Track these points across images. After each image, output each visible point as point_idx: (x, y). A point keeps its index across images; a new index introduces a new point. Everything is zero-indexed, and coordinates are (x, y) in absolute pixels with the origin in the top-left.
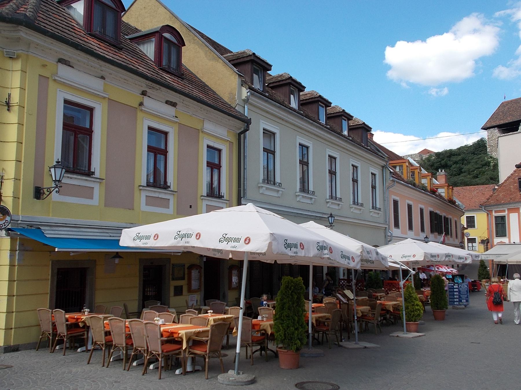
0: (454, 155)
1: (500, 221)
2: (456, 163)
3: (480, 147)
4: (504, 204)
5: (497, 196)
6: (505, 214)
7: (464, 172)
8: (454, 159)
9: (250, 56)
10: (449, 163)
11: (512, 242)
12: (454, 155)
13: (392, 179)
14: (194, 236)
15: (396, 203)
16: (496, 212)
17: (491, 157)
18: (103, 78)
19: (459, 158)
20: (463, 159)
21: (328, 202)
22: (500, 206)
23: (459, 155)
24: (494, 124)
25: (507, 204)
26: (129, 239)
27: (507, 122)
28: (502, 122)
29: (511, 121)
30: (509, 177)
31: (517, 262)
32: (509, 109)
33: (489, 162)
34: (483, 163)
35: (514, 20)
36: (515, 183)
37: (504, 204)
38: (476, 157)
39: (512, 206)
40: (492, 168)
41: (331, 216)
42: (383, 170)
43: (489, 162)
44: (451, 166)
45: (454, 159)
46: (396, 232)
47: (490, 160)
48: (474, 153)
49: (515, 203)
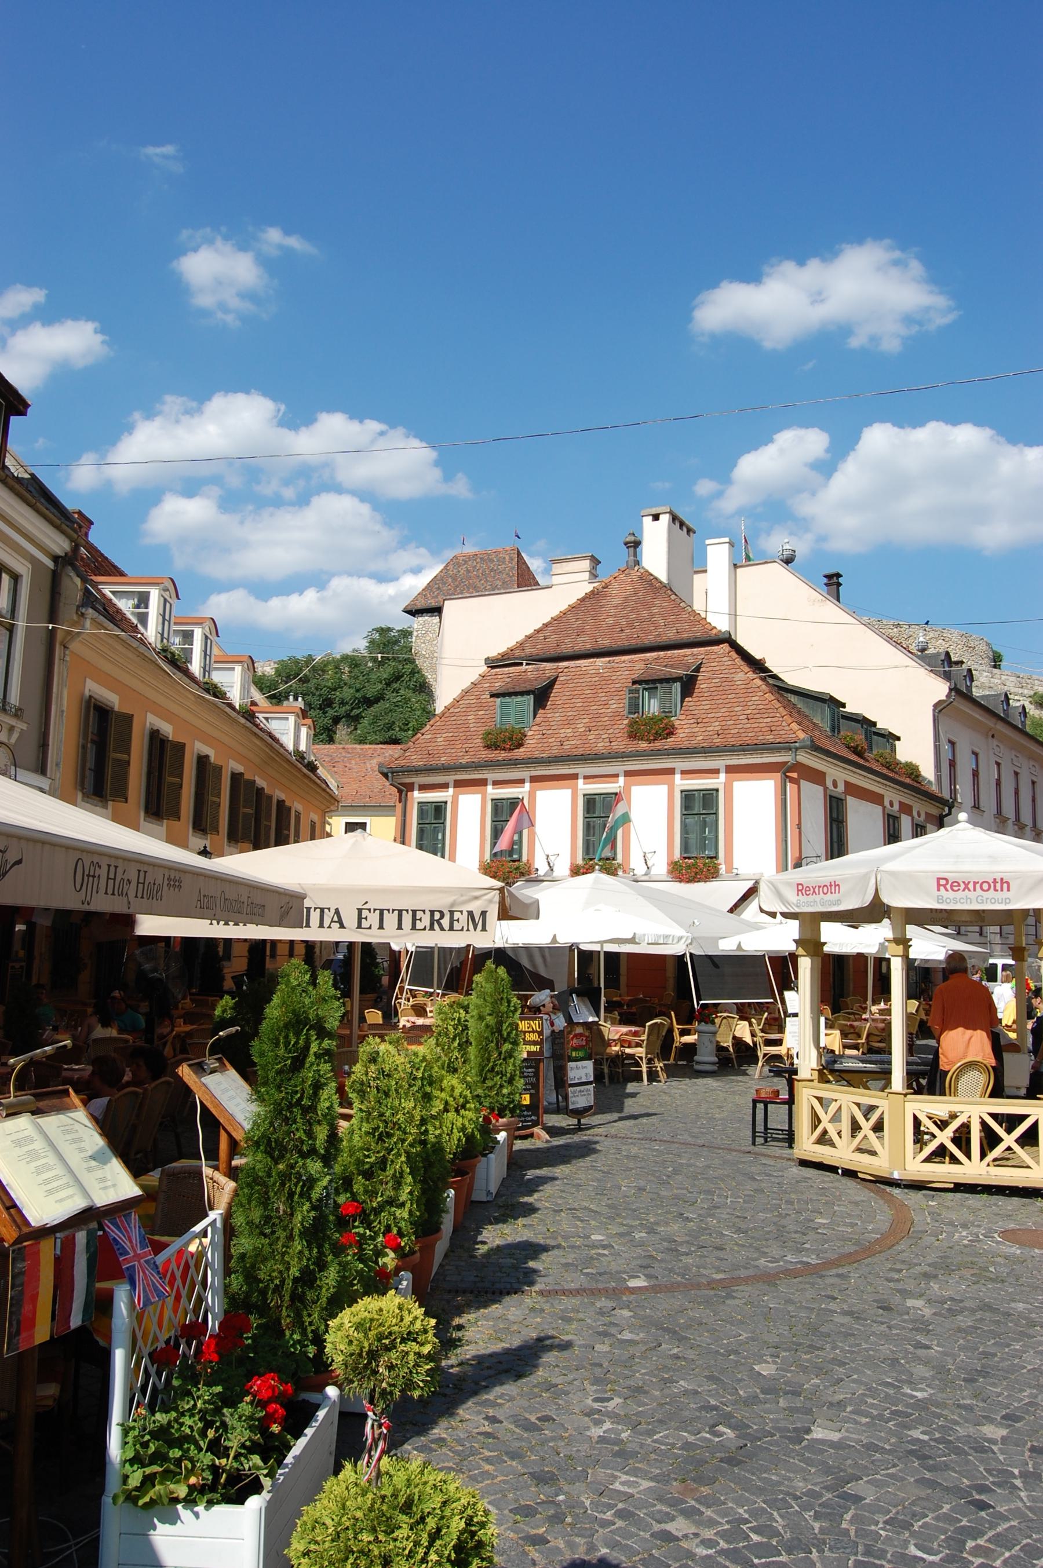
16: (423, 788)
32: (468, 571)
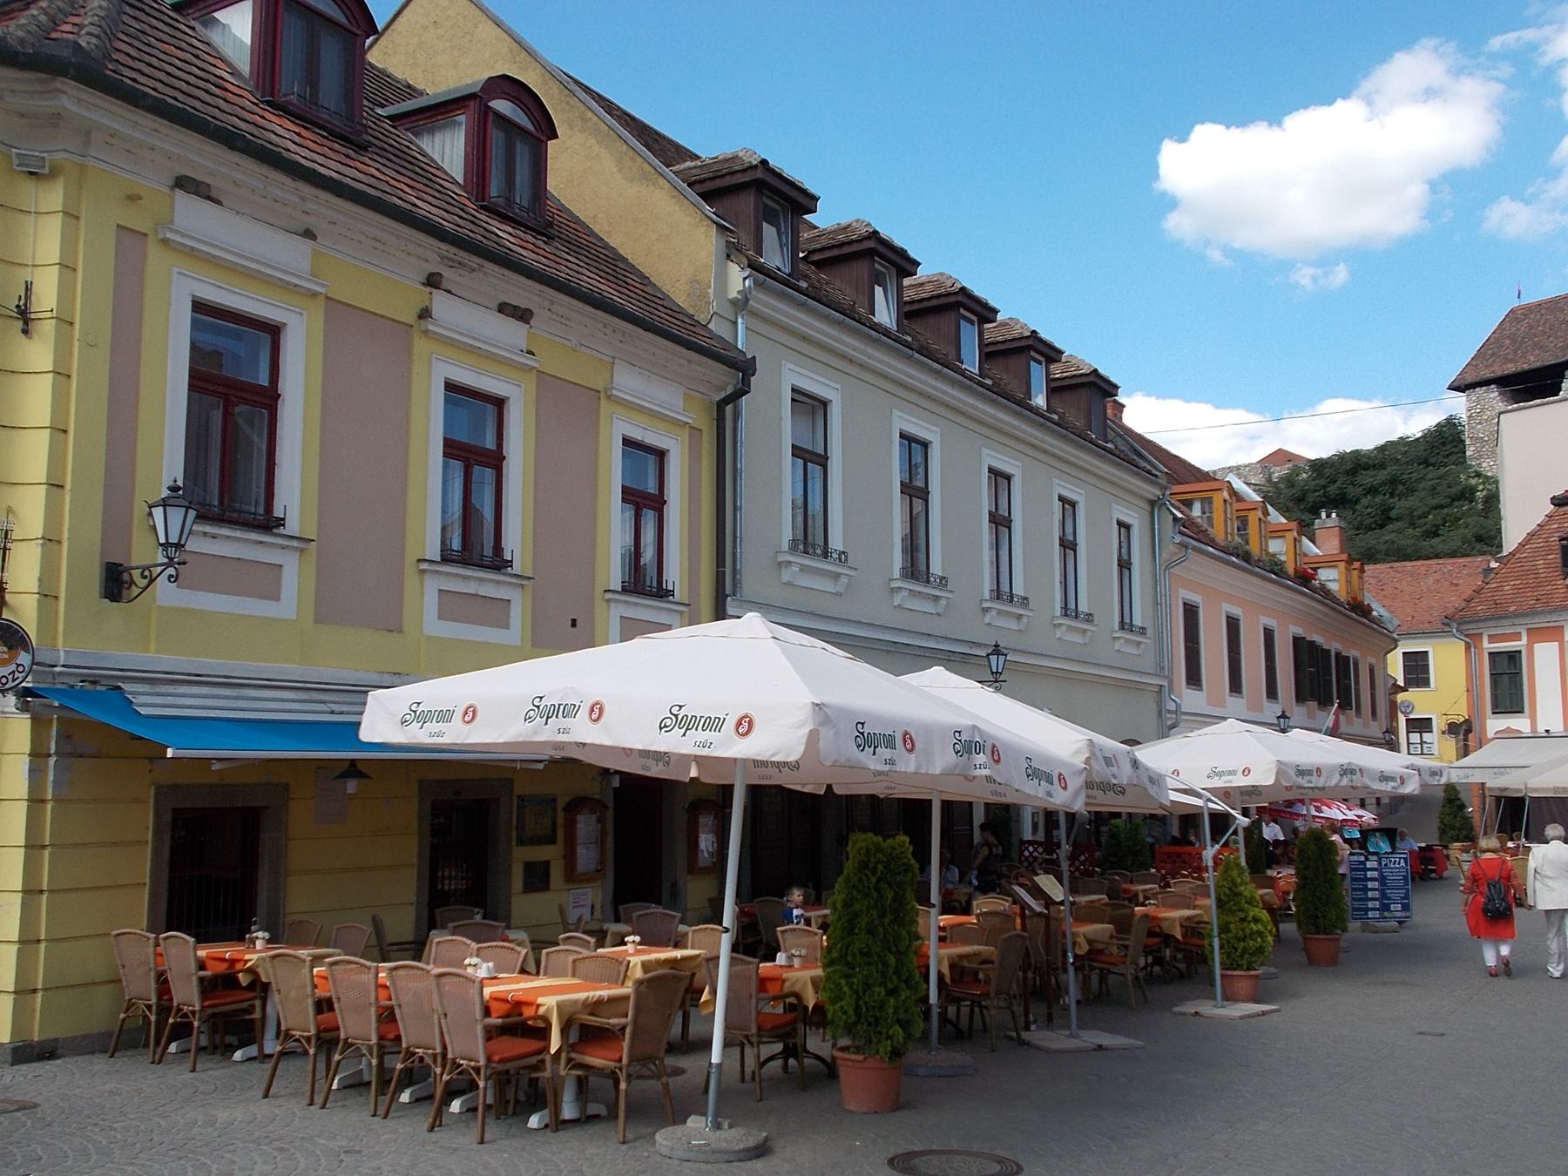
0: (1367, 467)
1: (1504, 666)
2: (1372, 490)
3: (1444, 444)
4: (1516, 615)
5: (1496, 590)
6: (1521, 644)
7: (1398, 519)
8: (1367, 478)
9: (753, 167)
10: (1352, 492)
11: (1541, 729)
12: (1367, 467)
13: (1178, 539)
14: (583, 713)
15: (1191, 612)
16: (1492, 639)
17: (1478, 475)
18: (309, 234)
19: (1383, 475)
20: (1394, 481)
21: (986, 610)
22: (1506, 622)
23: (1383, 466)
24: (1487, 374)
25: (1525, 615)
26: (388, 720)
27: (1526, 367)
28: (1511, 368)
29: (1538, 364)
30: (1531, 535)
31: (1556, 789)
32: (1531, 327)
33: (1473, 490)
34: (1454, 490)
35: (1546, 61)
36: (1549, 551)
37: (1516, 616)
38: (1432, 473)
39: (1541, 622)
40: (1480, 506)
41: (997, 650)
42: (1152, 513)
43: (1473, 490)
44: (1358, 501)
45: (1367, 478)
46: (1191, 700)
47: (1473, 482)
48: (1426, 463)
49: (1550, 612)
